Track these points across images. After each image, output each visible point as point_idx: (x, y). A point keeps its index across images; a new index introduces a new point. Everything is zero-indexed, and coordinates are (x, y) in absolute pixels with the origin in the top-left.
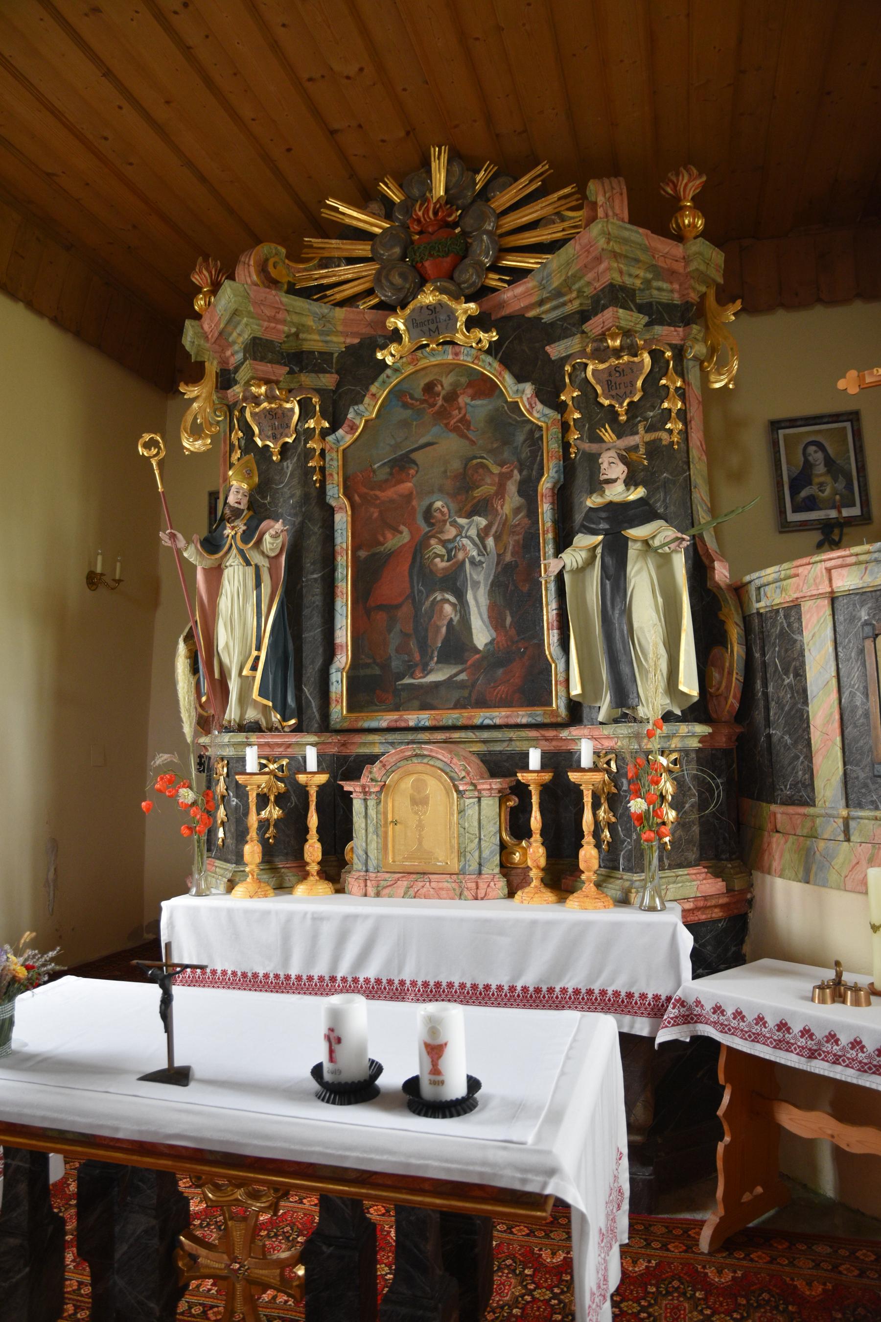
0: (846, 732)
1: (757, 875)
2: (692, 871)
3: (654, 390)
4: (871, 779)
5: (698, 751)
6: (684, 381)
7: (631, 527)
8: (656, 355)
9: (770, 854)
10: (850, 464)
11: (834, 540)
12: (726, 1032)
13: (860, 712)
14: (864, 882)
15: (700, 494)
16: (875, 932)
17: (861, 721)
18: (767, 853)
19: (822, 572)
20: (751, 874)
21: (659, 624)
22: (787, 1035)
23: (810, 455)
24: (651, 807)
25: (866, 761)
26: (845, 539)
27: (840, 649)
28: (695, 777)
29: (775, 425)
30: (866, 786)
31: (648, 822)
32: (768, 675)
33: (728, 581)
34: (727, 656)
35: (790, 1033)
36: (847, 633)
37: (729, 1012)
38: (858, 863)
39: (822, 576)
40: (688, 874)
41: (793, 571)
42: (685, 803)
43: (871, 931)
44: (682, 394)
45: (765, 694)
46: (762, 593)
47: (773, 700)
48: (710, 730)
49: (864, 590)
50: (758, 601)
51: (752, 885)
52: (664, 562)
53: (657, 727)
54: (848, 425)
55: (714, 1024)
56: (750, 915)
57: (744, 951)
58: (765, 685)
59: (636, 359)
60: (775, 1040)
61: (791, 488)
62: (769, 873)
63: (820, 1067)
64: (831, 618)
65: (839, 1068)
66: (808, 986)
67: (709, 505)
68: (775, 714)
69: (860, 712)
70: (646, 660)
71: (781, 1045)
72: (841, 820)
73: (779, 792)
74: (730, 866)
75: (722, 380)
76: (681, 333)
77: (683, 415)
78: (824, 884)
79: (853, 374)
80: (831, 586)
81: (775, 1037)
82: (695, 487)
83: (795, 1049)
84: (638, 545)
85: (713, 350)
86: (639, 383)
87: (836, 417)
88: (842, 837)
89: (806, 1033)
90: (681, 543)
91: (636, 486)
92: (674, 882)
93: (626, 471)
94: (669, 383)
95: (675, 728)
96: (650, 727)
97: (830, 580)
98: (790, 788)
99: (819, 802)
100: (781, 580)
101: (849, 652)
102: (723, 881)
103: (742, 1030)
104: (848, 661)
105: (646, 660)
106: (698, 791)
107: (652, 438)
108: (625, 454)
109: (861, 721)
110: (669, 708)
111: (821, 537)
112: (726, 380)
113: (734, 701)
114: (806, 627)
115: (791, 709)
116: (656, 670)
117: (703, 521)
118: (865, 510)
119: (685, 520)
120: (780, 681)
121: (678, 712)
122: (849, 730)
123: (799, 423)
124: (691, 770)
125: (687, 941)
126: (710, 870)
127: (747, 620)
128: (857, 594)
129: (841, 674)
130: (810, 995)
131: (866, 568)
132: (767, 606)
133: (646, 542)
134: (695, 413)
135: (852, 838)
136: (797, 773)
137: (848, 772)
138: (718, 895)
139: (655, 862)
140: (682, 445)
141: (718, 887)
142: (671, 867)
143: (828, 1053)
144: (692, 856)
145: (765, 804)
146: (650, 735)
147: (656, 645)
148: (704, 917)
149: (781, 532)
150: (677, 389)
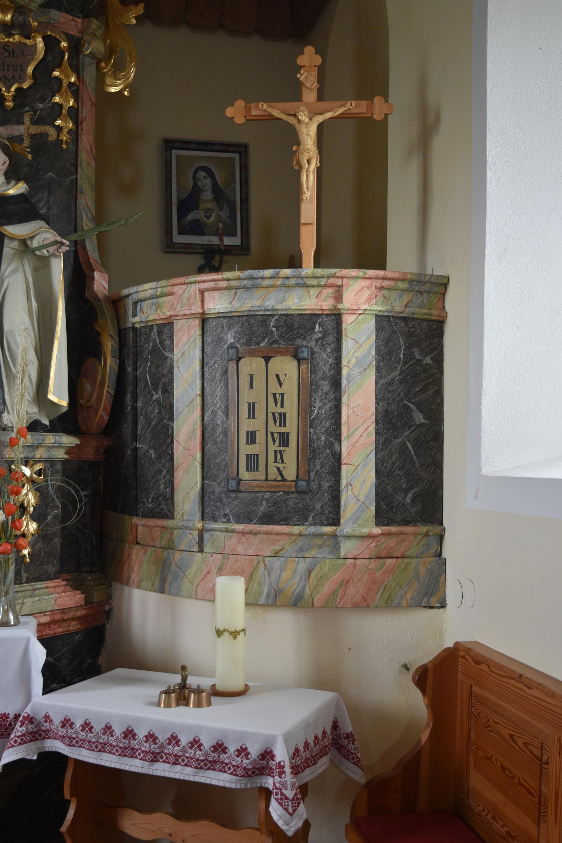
0: (206, 449)
1: (116, 586)
2: (51, 584)
3: (44, 82)
4: (225, 493)
5: (64, 462)
6: (78, 77)
7: (10, 222)
8: (51, 43)
9: (129, 566)
10: (235, 195)
11: (214, 266)
12: (74, 746)
13: (220, 430)
14: (213, 591)
15: (86, 200)
16: (219, 636)
17: (220, 438)
18: (126, 565)
19: (195, 293)
20: (111, 586)
21: (30, 327)
22: (132, 742)
23: (199, 180)
24: (10, 518)
25: (222, 476)
26: (224, 266)
27: (206, 369)
28: (60, 489)
29: (169, 144)
30: (220, 499)
31: (6, 533)
32: (138, 390)
33: (106, 293)
34: (100, 368)
35: (135, 739)
36: (213, 354)
37: (78, 724)
38: (209, 573)
39: (195, 296)
40: (47, 588)
41: (168, 290)
42: (48, 515)
43: (216, 635)
44: (75, 91)
45: (135, 409)
46: (139, 308)
47: (141, 415)
48: (78, 442)
49: (232, 315)
50: (134, 315)
51: (111, 597)
52: (42, 266)
53: (21, 436)
54: (237, 156)
55: (62, 738)
56: (108, 626)
57: (99, 663)
58: (135, 399)
59: (28, 42)
60: (121, 748)
61: (179, 209)
62: (128, 584)
63: (162, 769)
64: (200, 338)
65: (178, 768)
66: (154, 692)
67: (94, 214)
68: (143, 428)
69: (220, 430)
70: (15, 366)
71: (127, 752)
72: (196, 532)
73: (142, 505)
74: (90, 578)
75: (118, 85)
76: (80, 25)
77: (74, 114)
78: (178, 593)
79: (240, 103)
80: (203, 308)
81: (121, 745)
82: (81, 192)
83: (139, 754)
84: (15, 244)
85: (111, 51)
86: (30, 70)
87: (226, 147)
88: (196, 548)
89: (151, 737)
90: (60, 247)
91: (18, 180)
92: (31, 596)
93: (7, 163)
94: (62, 77)
95: (43, 437)
96: (14, 435)
97: (203, 302)
98: (152, 501)
99: (177, 515)
100: (158, 297)
101: (212, 373)
102: (82, 593)
103: (89, 742)
104: (213, 381)
105: (15, 366)
106: (62, 503)
107: (38, 131)
108: (7, 143)
109: (220, 438)
110: (37, 417)
111: (203, 262)
112: (122, 86)
113: (104, 414)
114: (178, 344)
115: (158, 424)
116: (23, 376)
117: (85, 228)
118: (244, 240)
119: (66, 224)
120: (149, 396)
121: (46, 422)
122: (208, 446)
123: (192, 146)
124: (55, 481)
125: (39, 654)
126: (70, 583)
127: (122, 333)
128: (226, 317)
129: (206, 393)
130: (157, 700)
131: (236, 294)
132: (142, 322)
133: (23, 242)
134: (87, 113)
135: (206, 549)
136: (159, 486)
137: (206, 486)
138: (77, 608)
139: (11, 575)
140: (71, 146)
141: (76, 599)
142: (28, 581)
143: (170, 754)
144: (52, 569)
145: (127, 517)
146: (13, 443)
147: (25, 351)
148: (60, 630)
149: (166, 252)
150: (70, 84)
